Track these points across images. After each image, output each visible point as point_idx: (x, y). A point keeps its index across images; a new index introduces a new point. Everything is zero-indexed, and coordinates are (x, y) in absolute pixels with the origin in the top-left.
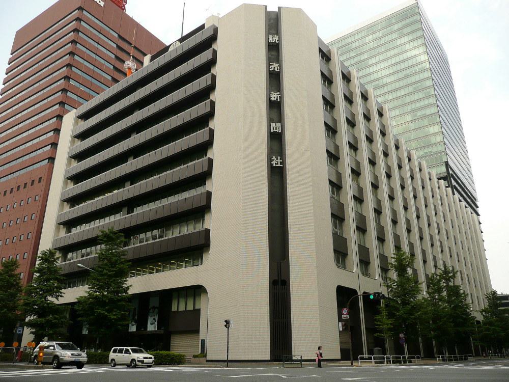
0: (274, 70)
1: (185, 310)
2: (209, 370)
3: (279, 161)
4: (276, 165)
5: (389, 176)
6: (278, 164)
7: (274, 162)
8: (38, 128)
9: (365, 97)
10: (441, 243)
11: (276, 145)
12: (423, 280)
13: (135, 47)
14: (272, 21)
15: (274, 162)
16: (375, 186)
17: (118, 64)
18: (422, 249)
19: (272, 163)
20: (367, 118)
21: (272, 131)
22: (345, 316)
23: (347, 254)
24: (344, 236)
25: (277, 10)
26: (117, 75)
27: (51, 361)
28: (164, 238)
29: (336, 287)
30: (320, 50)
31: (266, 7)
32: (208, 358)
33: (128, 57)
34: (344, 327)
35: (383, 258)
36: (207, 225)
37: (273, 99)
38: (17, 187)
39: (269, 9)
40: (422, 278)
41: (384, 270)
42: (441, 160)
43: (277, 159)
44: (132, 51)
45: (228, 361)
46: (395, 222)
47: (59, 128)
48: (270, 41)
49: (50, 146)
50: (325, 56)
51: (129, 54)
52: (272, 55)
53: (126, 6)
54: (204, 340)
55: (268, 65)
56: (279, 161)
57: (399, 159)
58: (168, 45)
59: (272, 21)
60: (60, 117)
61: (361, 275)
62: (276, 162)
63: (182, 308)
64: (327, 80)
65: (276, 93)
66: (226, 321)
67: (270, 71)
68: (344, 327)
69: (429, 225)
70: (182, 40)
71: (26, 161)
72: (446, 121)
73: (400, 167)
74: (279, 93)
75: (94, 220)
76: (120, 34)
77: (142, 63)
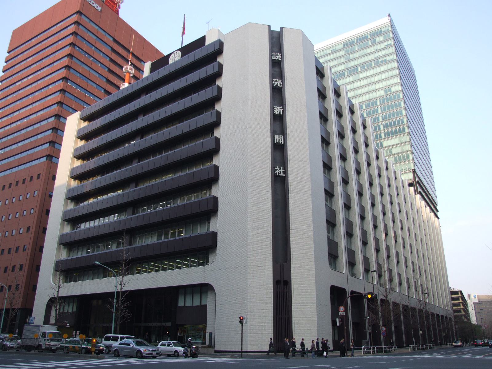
0: (277, 85)
1: (191, 305)
2: (253, 361)
4: (279, 175)
5: (358, 172)
6: (280, 173)
7: (277, 172)
8: (36, 126)
9: (337, 93)
10: (403, 239)
11: (278, 154)
12: (375, 269)
14: (274, 40)
15: (277, 172)
16: (345, 182)
19: (276, 172)
20: (339, 114)
21: (275, 142)
22: (342, 313)
23: (338, 257)
24: (335, 240)
25: (279, 30)
27: (173, 354)
28: (177, 238)
29: (330, 286)
30: (317, 68)
31: (269, 26)
32: (217, 348)
34: (341, 323)
36: (213, 227)
37: (276, 112)
38: (15, 182)
39: (272, 29)
43: (280, 169)
44: (130, 58)
45: (242, 352)
46: (363, 218)
48: (273, 58)
49: (48, 144)
50: (320, 73)
51: (127, 61)
52: (274, 71)
53: (120, 11)
54: (212, 333)
55: (272, 81)
56: (282, 170)
57: (368, 157)
58: (166, 54)
59: (274, 40)
62: (279, 171)
63: (188, 304)
64: (322, 95)
65: (279, 108)
66: (240, 318)
68: (341, 323)
69: (394, 222)
70: (185, 50)
71: (25, 157)
73: (369, 164)
74: (281, 107)
75: (99, 218)
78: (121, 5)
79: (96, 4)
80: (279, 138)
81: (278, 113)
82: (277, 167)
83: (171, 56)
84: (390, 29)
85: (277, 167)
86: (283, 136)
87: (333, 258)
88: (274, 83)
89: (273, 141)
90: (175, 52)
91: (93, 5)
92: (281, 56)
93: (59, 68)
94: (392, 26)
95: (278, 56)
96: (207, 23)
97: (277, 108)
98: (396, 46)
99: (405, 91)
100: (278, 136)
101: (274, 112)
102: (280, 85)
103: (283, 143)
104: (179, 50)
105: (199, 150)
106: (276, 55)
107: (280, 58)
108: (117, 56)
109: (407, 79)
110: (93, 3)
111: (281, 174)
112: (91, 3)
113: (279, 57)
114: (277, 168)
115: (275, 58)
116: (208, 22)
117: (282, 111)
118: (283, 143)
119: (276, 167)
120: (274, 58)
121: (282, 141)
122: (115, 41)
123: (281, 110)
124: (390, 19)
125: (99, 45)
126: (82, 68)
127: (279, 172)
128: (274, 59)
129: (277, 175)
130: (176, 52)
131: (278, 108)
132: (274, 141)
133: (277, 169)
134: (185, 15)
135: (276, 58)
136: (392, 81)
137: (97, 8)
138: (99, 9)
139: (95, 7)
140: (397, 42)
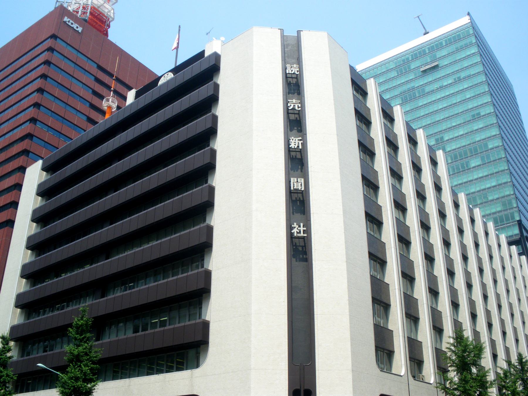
3: (302, 229)
4: (298, 235)
7: (295, 231)
13: (118, 80)
15: (295, 231)
17: (95, 101)
18: (491, 339)
19: (293, 231)
21: (292, 188)
26: (94, 115)
33: (108, 91)
35: (439, 353)
37: (291, 118)
40: (491, 377)
41: (442, 370)
42: (513, 218)
43: (300, 226)
44: (113, 85)
47: (17, 201)
48: (287, 72)
51: (109, 87)
56: (302, 229)
58: (160, 75)
60: (22, 169)
61: (411, 378)
62: (298, 230)
65: (297, 139)
67: (288, 110)
70: (176, 70)
72: (516, 167)
74: (300, 138)
76: (100, 64)
77: (125, 98)
78: (111, 23)
79: (76, 24)
80: (297, 182)
81: (296, 147)
82: (295, 224)
83: (160, 80)
84: (471, 32)
85: (295, 224)
86: (303, 180)
87: (412, 320)
88: (289, 105)
89: (288, 188)
90: (166, 75)
91: (72, 26)
92: (299, 68)
93: (27, 107)
94: (473, 28)
95: (294, 69)
96: (207, 34)
97: (294, 140)
98: (482, 54)
99: (499, 112)
100: (296, 179)
101: (290, 146)
102: (299, 107)
103: (303, 189)
104: (170, 71)
105: (187, 205)
106: (291, 67)
107: (297, 71)
108: (102, 87)
109: (502, 99)
110: (72, 24)
111: (300, 234)
112: (70, 24)
113: (296, 69)
114: (295, 225)
115: (290, 71)
116: (208, 32)
117: (302, 143)
118: (303, 189)
119: (294, 224)
120: (289, 71)
121: (301, 186)
122: (100, 68)
123: (300, 142)
124: (470, 19)
125: (79, 74)
126: (56, 106)
127: (298, 231)
128: (289, 73)
129: (295, 235)
130: (167, 75)
131: (295, 140)
132: (290, 187)
133: (295, 227)
134: (180, 27)
135: (292, 71)
136: (480, 101)
137: (77, 29)
138: (80, 29)
139: (75, 28)
140: (488, 56)
